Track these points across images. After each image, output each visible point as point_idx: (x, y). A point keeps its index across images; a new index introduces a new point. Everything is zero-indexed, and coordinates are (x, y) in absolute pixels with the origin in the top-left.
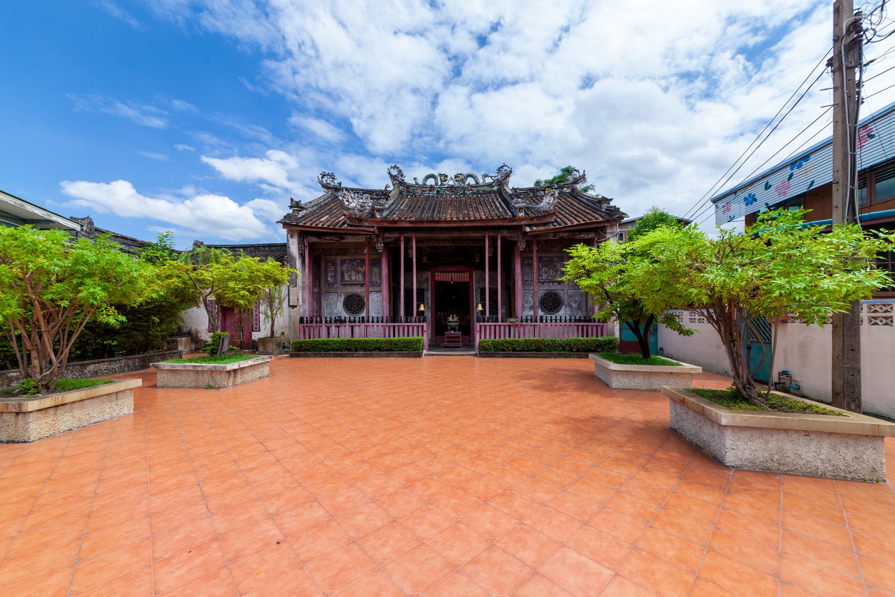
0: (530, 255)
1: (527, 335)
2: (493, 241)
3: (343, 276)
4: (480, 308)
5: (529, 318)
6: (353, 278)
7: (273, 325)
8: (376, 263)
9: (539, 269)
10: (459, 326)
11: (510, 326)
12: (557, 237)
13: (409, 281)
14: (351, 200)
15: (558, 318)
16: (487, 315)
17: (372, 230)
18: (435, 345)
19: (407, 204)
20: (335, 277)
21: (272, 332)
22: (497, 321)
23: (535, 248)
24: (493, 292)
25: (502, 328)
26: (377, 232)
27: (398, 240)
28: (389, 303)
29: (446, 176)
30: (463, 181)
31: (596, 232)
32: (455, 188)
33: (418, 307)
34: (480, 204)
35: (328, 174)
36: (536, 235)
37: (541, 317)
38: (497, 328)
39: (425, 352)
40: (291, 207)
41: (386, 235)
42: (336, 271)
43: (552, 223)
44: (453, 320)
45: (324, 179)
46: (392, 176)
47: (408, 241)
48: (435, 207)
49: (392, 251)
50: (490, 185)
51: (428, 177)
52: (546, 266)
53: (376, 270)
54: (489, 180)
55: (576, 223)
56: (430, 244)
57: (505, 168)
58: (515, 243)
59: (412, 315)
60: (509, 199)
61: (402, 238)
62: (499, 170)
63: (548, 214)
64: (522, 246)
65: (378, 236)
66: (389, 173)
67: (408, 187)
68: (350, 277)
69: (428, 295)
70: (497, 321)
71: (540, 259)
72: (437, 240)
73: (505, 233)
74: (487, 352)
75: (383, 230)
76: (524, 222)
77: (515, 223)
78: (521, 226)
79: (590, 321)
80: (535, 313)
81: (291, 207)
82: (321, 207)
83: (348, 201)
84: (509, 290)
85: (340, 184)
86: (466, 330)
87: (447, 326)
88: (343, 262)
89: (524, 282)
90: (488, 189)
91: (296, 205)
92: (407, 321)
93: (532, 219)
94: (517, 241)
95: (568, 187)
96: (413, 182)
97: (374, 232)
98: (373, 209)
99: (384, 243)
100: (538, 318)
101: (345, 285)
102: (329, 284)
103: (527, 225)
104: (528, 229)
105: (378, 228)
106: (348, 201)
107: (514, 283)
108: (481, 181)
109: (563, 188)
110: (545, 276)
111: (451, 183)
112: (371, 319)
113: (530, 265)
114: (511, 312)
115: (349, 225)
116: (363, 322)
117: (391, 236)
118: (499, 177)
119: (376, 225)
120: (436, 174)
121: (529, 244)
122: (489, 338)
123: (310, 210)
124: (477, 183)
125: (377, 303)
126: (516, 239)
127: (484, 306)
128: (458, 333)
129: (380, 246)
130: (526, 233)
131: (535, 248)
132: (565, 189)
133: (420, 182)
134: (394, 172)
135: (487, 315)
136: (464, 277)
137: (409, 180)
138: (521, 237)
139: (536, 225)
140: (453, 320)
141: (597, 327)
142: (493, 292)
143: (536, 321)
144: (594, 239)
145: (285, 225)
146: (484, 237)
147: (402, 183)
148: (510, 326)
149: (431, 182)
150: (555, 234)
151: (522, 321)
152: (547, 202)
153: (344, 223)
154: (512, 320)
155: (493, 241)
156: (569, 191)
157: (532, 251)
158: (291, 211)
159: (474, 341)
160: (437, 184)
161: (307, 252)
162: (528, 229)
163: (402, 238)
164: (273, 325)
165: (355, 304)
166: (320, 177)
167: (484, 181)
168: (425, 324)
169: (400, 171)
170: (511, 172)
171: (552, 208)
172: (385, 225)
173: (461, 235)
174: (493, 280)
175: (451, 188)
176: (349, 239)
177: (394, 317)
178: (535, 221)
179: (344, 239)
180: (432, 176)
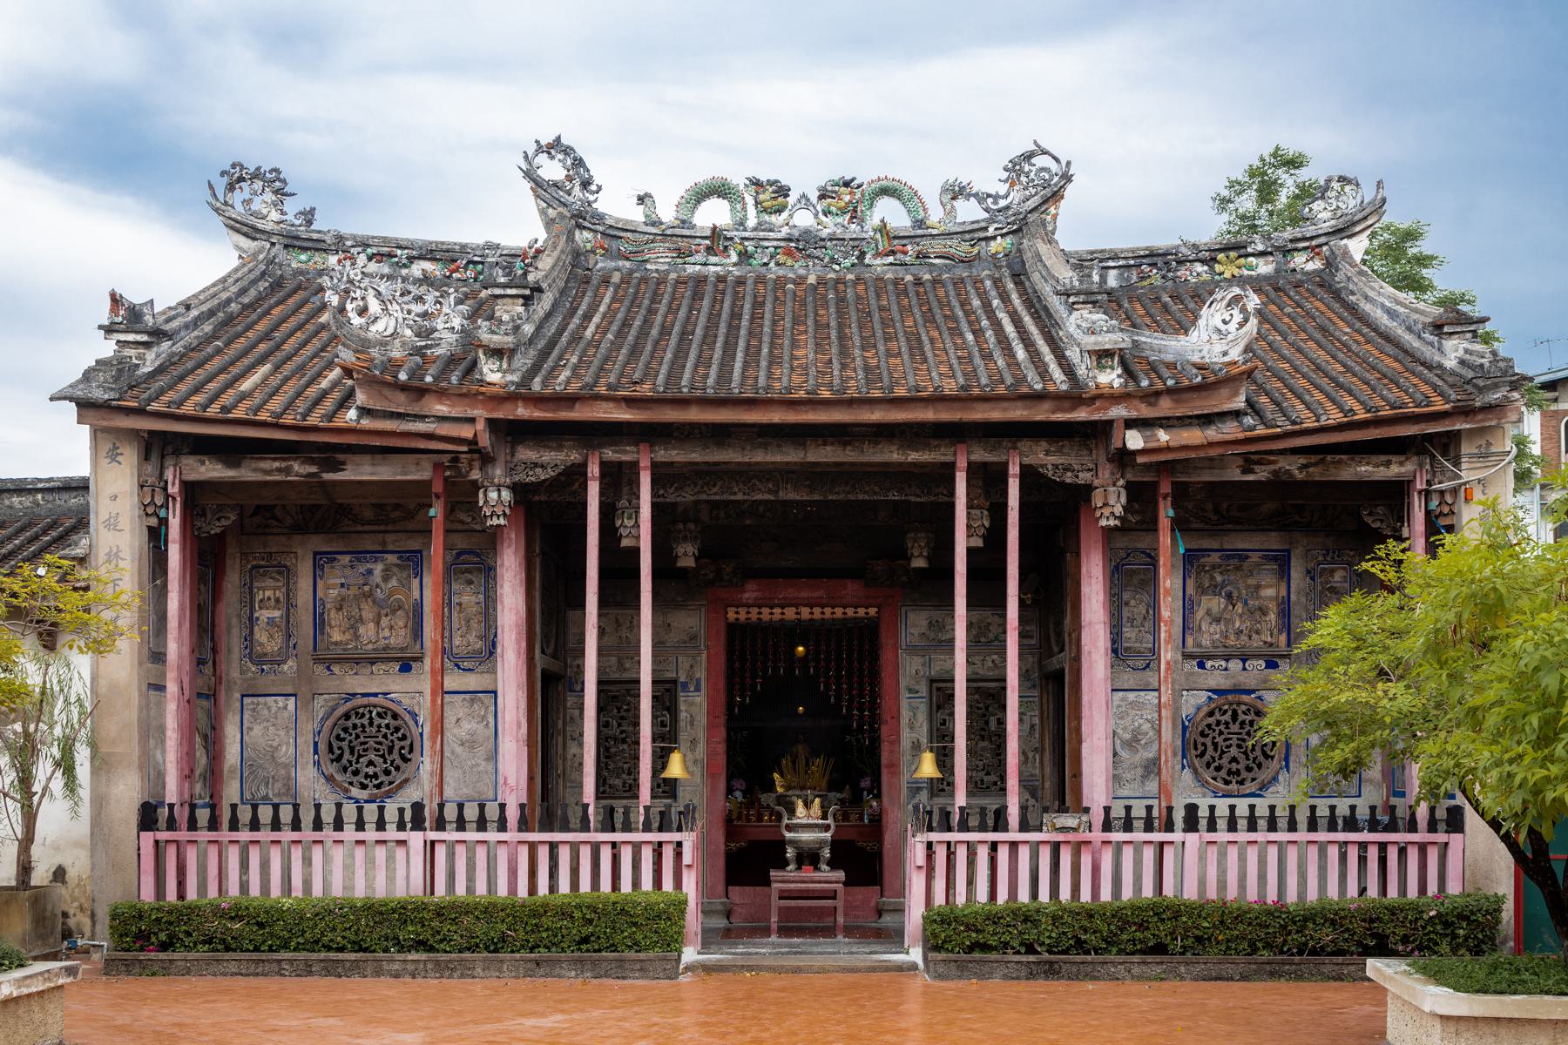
0: (1143, 542)
1: (1122, 874)
2: (988, 481)
3: (319, 623)
4: (928, 767)
5: (1139, 811)
6: (367, 631)
7: (27, 841)
8: (474, 562)
9: (1188, 608)
10: (835, 844)
11: (1056, 847)
12: (1261, 474)
13: (619, 647)
14: (374, 306)
15: (1262, 810)
16: (961, 799)
17: (466, 432)
18: (729, 928)
19: (610, 315)
20: (287, 628)
21: (25, 868)
22: (1000, 823)
23: (1166, 512)
24: (988, 698)
25: (1024, 854)
26: (485, 441)
27: (577, 474)
28: (530, 744)
29: (783, 191)
30: (854, 214)
31: (1421, 451)
32: (820, 242)
33: (661, 759)
34: (929, 319)
35: (257, 175)
36: (1169, 465)
37: (1192, 809)
38: (1003, 854)
39: (690, 954)
40: (109, 330)
41: (526, 454)
42: (289, 605)
43: (1237, 414)
44: (808, 822)
45: (237, 198)
46: (538, 185)
47: (618, 481)
48: (733, 329)
49: (550, 522)
50: (975, 234)
51: (702, 194)
52: (1215, 589)
53: (469, 598)
54: (969, 212)
55: (1335, 417)
56: (715, 494)
57: (1040, 161)
58: (1084, 493)
59: (632, 791)
60: (1056, 304)
61: (594, 470)
62: (1016, 168)
63: (1214, 381)
64: (1111, 504)
65: (486, 459)
66: (530, 175)
67: (613, 232)
68: (354, 625)
69: (696, 707)
70: (1000, 823)
71: (1191, 560)
72: (745, 474)
73: (1044, 457)
74: (965, 940)
75: (512, 432)
76: (1118, 412)
77: (1081, 415)
78: (1110, 423)
79: (1392, 827)
80: (1163, 791)
81: (109, 330)
82: (230, 320)
83: (362, 311)
84: (1055, 687)
85: (309, 216)
86: (864, 860)
87: (782, 844)
88: (321, 562)
89: (1118, 651)
90: (962, 249)
91: (127, 317)
92: (608, 825)
93: (1152, 396)
94: (1089, 488)
95: (1315, 251)
96: (636, 215)
97: (473, 442)
98: (468, 340)
99: (515, 488)
100: (1179, 816)
101: (328, 662)
102: (260, 660)
103: (1130, 424)
104: (1134, 440)
105: (492, 424)
106: (362, 311)
107: (1077, 659)
108: (935, 215)
109: (1286, 252)
110: (1209, 635)
111: (804, 219)
112: (450, 813)
113: (1149, 581)
114: (1058, 786)
115: (365, 412)
116: (418, 824)
117: (548, 456)
118: (1015, 196)
119: (480, 413)
120: (738, 180)
121: (1141, 497)
122: (973, 893)
123: (191, 337)
124: (920, 223)
125: (484, 735)
126: (1084, 477)
127: (944, 759)
128: (825, 872)
129: (496, 499)
130: (1124, 457)
131: (1166, 512)
132: (1299, 260)
133: (667, 213)
134: (552, 170)
135: (961, 799)
136: (845, 607)
137: (615, 204)
138: (1106, 473)
139: (1166, 423)
140: (808, 822)
141: (1423, 848)
142: (988, 698)
143: (1169, 827)
144: (1411, 482)
145: (86, 407)
146: (950, 468)
147: (583, 217)
148: (1056, 847)
149: (714, 214)
150: (1248, 464)
151: (1107, 826)
152: (1217, 336)
153: (343, 404)
154: (1069, 820)
155: (988, 481)
156: (1315, 265)
157: (1151, 526)
158: (108, 349)
159: (900, 910)
160: (741, 224)
161: (175, 523)
162: (1134, 440)
163: (594, 470)
164: (27, 841)
165: (370, 750)
166: (221, 184)
167: (951, 213)
168: (688, 839)
169: (579, 163)
170: (1067, 178)
171: (1235, 354)
172: (522, 412)
173: (849, 455)
174: (986, 640)
175: (803, 244)
176: (360, 471)
177: (548, 805)
178: (1166, 407)
179: (337, 467)
180: (719, 190)
